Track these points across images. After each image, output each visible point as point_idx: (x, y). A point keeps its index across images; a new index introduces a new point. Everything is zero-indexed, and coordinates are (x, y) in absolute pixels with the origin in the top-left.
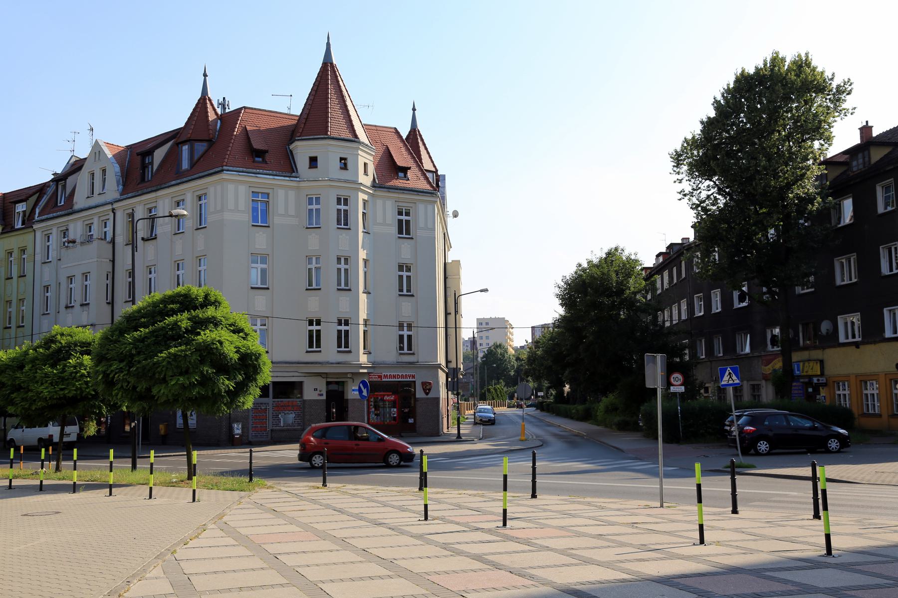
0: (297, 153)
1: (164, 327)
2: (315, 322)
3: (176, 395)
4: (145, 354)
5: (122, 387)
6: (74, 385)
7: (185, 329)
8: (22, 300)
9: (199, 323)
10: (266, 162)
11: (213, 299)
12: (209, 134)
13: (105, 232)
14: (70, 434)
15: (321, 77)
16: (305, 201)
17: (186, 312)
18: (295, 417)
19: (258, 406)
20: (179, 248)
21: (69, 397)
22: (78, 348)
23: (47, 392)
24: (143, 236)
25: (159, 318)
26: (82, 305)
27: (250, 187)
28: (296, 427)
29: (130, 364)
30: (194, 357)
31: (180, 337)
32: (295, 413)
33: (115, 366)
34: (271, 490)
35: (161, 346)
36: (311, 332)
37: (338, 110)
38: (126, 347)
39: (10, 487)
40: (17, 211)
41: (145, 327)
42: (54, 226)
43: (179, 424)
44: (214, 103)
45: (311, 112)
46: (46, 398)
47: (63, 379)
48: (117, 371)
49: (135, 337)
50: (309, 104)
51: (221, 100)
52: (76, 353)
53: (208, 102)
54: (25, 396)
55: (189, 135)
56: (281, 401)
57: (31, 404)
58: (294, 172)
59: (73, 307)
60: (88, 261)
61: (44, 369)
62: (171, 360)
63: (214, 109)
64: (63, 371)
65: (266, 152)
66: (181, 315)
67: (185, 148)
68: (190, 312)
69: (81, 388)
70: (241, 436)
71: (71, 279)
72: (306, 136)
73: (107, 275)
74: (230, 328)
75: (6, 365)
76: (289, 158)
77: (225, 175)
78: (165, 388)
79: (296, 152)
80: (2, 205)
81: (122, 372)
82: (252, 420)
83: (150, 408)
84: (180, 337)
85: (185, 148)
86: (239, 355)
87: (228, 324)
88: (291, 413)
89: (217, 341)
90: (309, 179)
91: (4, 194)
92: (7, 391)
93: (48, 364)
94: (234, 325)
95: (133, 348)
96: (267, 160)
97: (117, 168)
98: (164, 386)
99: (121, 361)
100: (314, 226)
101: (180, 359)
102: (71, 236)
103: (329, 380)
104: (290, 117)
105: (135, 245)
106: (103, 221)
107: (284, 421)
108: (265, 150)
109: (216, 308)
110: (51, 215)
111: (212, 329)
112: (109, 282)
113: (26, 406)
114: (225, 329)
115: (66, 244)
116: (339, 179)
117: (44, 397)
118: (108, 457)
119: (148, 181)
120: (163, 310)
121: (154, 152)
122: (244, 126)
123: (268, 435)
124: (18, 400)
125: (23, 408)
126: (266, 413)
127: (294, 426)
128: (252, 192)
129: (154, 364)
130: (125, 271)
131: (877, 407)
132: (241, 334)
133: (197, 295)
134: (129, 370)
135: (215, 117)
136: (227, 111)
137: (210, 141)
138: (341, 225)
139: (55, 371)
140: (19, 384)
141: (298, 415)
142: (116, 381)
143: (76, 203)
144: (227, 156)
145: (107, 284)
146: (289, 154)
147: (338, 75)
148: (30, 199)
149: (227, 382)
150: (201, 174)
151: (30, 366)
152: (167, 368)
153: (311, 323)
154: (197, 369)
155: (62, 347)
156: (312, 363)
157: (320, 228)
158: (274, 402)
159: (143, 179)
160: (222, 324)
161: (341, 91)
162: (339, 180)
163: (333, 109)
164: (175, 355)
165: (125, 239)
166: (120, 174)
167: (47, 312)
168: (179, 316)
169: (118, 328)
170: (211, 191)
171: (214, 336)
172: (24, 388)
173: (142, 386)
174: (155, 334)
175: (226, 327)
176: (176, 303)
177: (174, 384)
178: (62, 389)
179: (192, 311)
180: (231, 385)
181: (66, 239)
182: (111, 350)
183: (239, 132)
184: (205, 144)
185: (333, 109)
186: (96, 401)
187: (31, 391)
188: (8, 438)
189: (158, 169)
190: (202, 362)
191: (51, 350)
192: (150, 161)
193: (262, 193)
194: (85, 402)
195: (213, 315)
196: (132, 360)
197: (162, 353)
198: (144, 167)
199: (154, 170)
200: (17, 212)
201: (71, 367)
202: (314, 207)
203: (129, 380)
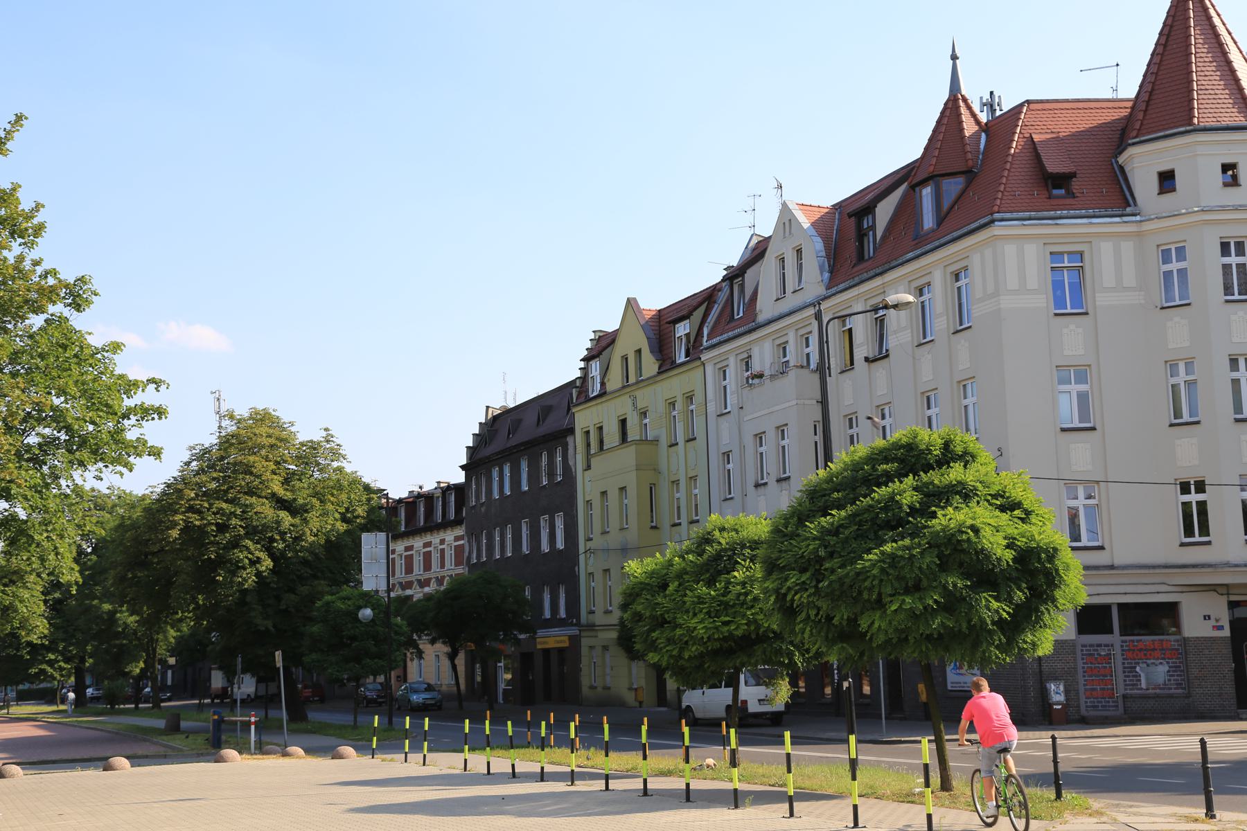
0: (1133, 168)
1: (871, 506)
2: (1193, 487)
3: (902, 631)
4: (841, 556)
5: (808, 616)
6: (744, 615)
7: (909, 507)
8: (693, 478)
9: (934, 495)
10: (1073, 193)
11: (959, 450)
12: (967, 161)
13: (808, 355)
15: (1173, 17)
16: (1154, 256)
17: (911, 476)
18: (1168, 671)
19: (1094, 650)
20: (928, 368)
21: (738, 636)
22: (747, 551)
23: (703, 628)
24: (866, 355)
25: (863, 490)
26: (779, 481)
27: (1044, 244)
28: (1173, 691)
29: (818, 576)
30: (928, 560)
31: (901, 522)
32: (1168, 663)
33: (792, 580)
34: (1096, 820)
35: (868, 541)
36: (1186, 505)
37: (1212, 73)
38: (809, 545)
39: (645, 792)
40: (677, 336)
41: (840, 507)
42: (730, 354)
43: (952, 683)
44: (972, 105)
45: (1156, 87)
46: (703, 638)
47: (726, 606)
48: (797, 588)
49: (823, 527)
50: (1152, 73)
51: (986, 97)
52: (745, 561)
53: (961, 103)
54: (672, 634)
55: (932, 168)
56: (1138, 641)
57: (682, 650)
58: (1130, 206)
59: (766, 484)
61: (696, 589)
63: (974, 115)
64: (726, 592)
65: (1072, 175)
66: (901, 482)
67: (927, 192)
68: (919, 476)
69: (755, 621)
70: (1066, 706)
71: (759, 437)
72: (1149, 133)
73: (815, 426)
74: (994, 501)
75: (641, 583)
76: (1119, 180)
77: (997, 230)
78: (881, 617)
79: (1129, 169)
80: (657, 328)
81: (807, 590)
82: (1084, 676)
83: (862, 654)
84: (901, 522)
85: (927, 192)
86: (1014, 553)
87: (990, 495)
88: (1161, 663)
89: (968, 528)
90: (1160, 215)
91: (659, 311)
92: (645, 626)
93: (703, 580)
94: (1002, 497)
95: (820, 546)
96: (1074, 191)
97: (819, 244)
98: (878, 614)
99: (803, 571)
100: (1178, 302)
101: (902, 563)
102: (756, 367)
103: (1233, 598)
104: (1117, 105)
105: (827, 365)
106: (802, 336)
107: (1147, 679)
108: (1070, 173)
109: (965, 466)
110: (725, 336)
111: (960, 505)
112: (819, 438)
113: (675, 653)
114: (986, 503)
115: (750, 381)
116: (1221, 206)
117: (699, 636)
119: (870, 258)
120: (870, 475)
121: (876, 206)
122: (1028, 135)
123: (1117, 706)
124: (661, 642)
125: (671, 656)
126: (1111, 663)
127: (1170, 689)
128: (1051, 253)
129: (858, 574)
130: (842, 418)
132: (1016, 512)
133: (929, 444)
134: (816, 587)
135: (976, 128)
136: (998, 113)
137: (970, 174)
138: (1233, 295)
139: (712, 593)
140: (661, 615)
141: (1176, 667)
142: (797, 607)
143: (761, 311)
144: (1000, 195)
145: (816, 443)
146: (1118, 173)
147: (1209, 6)
149: (995, 605)
150: (955, 234)
151: (676, 583)
152: (881, 581)
153: (1185, 489)
154: (936, 581)
155: (722, 550)
156: (1203, 566)
157: (1189, 304)
158: (1123, 642)
159: (861, 257)
160: (977, 495)
161: (1217, 36)
162: (1223, 209)
163: (1202, 74)
164: (893, 556)
165: (839, 362)
166: (823, 254)
167: (730, 496)
168: (898, 483)
169: (794, 513)
170: (975, 262)
171: (960, 516)
172: (669, 622)
173: (841, 616)
174: (857, 519)
175: (988, 501)
176: (893, 460)
177: (896, 610)
178: (726, 623)
179: (922, 473)
180: (1005, 610)
181: (749, 373)
182: (786, 551)
183: (1020, 147)
184: (960, 181)
185: (1202, 74)
186: (782, 642)
187: (680, 626)
188: (684, 705)
189: (884, 237)
190: (944, 567)
191: (705, 556)
192: (870, 224)
193: (1069, 253)
194: (765, 645)
195: (959, 479)
196: (820, 569)
197: (871, 553)
198: (861, 235)
199: (878, 238)
201: (738, 584)
202: (1174, 266)
203: (819, 603)
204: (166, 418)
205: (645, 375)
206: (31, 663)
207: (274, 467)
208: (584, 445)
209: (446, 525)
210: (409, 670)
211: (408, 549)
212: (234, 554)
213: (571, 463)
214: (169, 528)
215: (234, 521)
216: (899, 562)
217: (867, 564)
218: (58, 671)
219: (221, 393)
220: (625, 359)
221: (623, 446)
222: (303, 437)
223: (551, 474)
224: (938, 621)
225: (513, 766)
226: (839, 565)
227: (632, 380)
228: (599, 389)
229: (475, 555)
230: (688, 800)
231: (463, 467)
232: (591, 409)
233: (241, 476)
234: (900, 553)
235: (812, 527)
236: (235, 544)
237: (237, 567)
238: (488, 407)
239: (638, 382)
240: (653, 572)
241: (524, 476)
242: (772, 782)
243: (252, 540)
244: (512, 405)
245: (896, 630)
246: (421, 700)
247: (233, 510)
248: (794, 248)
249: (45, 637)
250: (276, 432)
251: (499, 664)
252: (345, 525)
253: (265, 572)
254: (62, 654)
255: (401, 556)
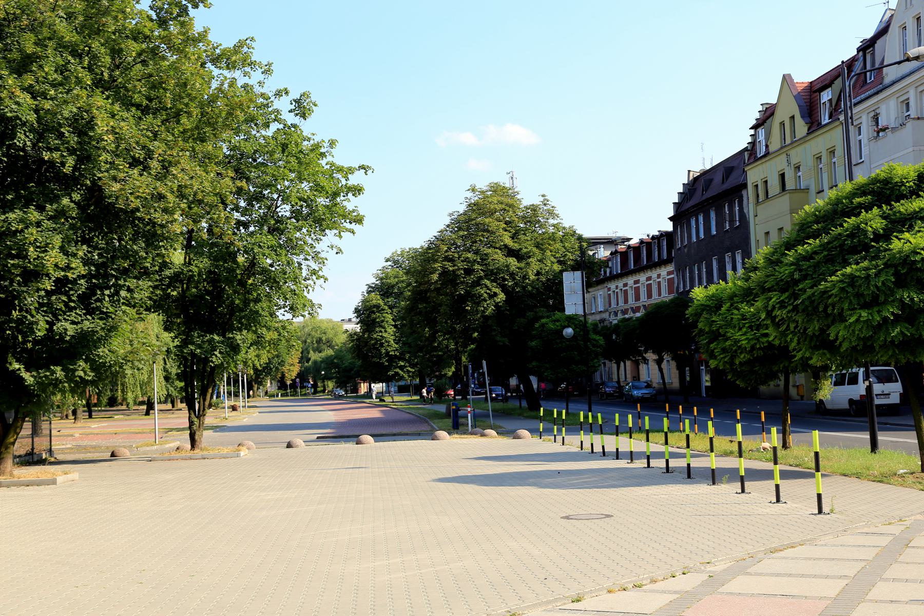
4: (813, 278)
14: (889, 394)
40: (822, 102)
57: (733, 358)
60: (902, 153)
62: (845, 285)
75: (702, 305)
81: (786, 307)
91: (811, 83)
95: (795, 270)
99: (783, 291)
101: (860, 282)
102: (882, 123)
118: (734, 433)
131: (828, 396)
148: (835, 82)
151: (728, 305)
164: (852, 277)
173: (814, 327)
200: (823, 103)
203: (797, 318)
204: (363, 193)
205: (798, 137)
206: (389, 368)
207: (505, 226)
208: (755, 196)
209: (661, 263)
210: (641, 372)
211: (636, 282)
212: (477, 290)
213: (745, 211)
214: (432, 273)
215: (476, 267)
216: (857, 281)
217: (829, 285)
218: (407, 374)
219: (514, 173)
220: (782, 124)
221: (783, 193)
222: (526, 202)
223: (732, 221)
224: (898, 330)
225: (603, 447)
226: (809, 286)
227: (788, 141)
228: (764, 150)
229: (682, 286)
230: (689, 477)
231: (671, 219)
232: (758, 167)
233: (480, 234)
234: (858, 274)
235: (791, 256)
236: (477, 283)
237: (478, 300)
238: (689, 171)
239: (792, 143)
240: (713, 296)
241: (713, 223)
242: (792, 461)
243: (488, 279)
244: (708, 167)
245: (859, 338)
246: (640, 395)
247: (475, 258)
248: (914, 17)
249: (397, 350)
250: (505, 200)
251: (702, 368)
252: (560, 267)
253: (500, 302)
254: (408, 361)
255: (632, 287)
